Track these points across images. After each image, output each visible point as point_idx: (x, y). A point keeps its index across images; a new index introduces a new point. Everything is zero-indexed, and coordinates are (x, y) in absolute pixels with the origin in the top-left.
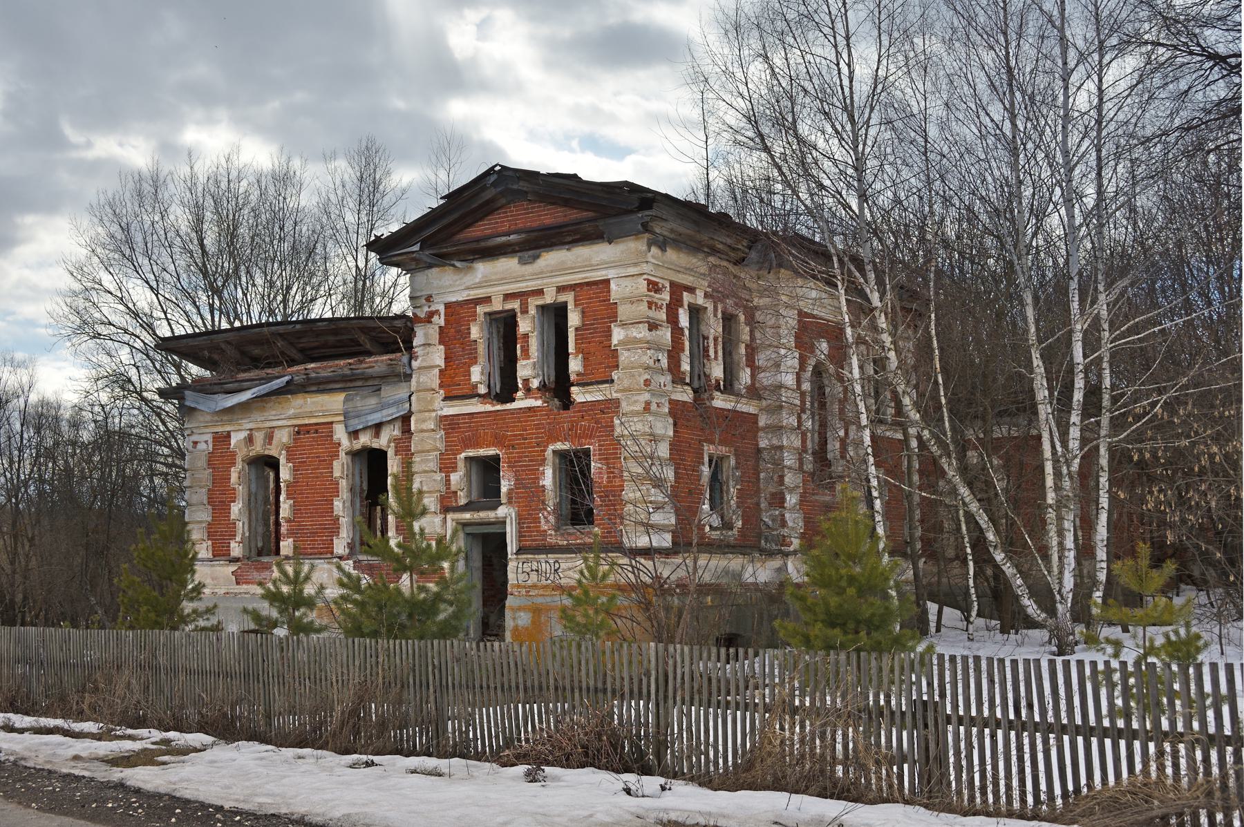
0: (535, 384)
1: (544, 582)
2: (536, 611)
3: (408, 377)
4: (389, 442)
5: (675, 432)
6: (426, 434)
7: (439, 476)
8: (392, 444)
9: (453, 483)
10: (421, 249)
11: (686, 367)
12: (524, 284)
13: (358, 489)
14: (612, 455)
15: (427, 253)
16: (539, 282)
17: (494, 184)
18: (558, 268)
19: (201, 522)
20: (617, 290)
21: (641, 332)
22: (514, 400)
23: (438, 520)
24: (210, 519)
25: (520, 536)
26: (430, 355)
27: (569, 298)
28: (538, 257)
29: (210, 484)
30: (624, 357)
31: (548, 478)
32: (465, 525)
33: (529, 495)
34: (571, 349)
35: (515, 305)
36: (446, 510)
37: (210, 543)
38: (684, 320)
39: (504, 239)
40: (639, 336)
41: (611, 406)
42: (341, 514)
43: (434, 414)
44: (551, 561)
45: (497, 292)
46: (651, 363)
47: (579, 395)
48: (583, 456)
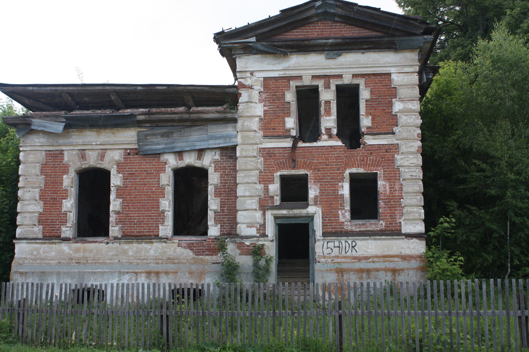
3: (235, 121)
4: (211, 163)
6: (250, 159)
7: (260, 187)
8: (213, 165)
12: (329, 71)
16: (340, 70)
18: (350, 65)
24: (41, 210)
25: (324, 225)
29: (42, 186)
31: (345, 190)
33: (330, 202)
40: (413, 108)
42: (167, 209)
43: (255, 147)
44: (350, 242)
48: (372, 179)
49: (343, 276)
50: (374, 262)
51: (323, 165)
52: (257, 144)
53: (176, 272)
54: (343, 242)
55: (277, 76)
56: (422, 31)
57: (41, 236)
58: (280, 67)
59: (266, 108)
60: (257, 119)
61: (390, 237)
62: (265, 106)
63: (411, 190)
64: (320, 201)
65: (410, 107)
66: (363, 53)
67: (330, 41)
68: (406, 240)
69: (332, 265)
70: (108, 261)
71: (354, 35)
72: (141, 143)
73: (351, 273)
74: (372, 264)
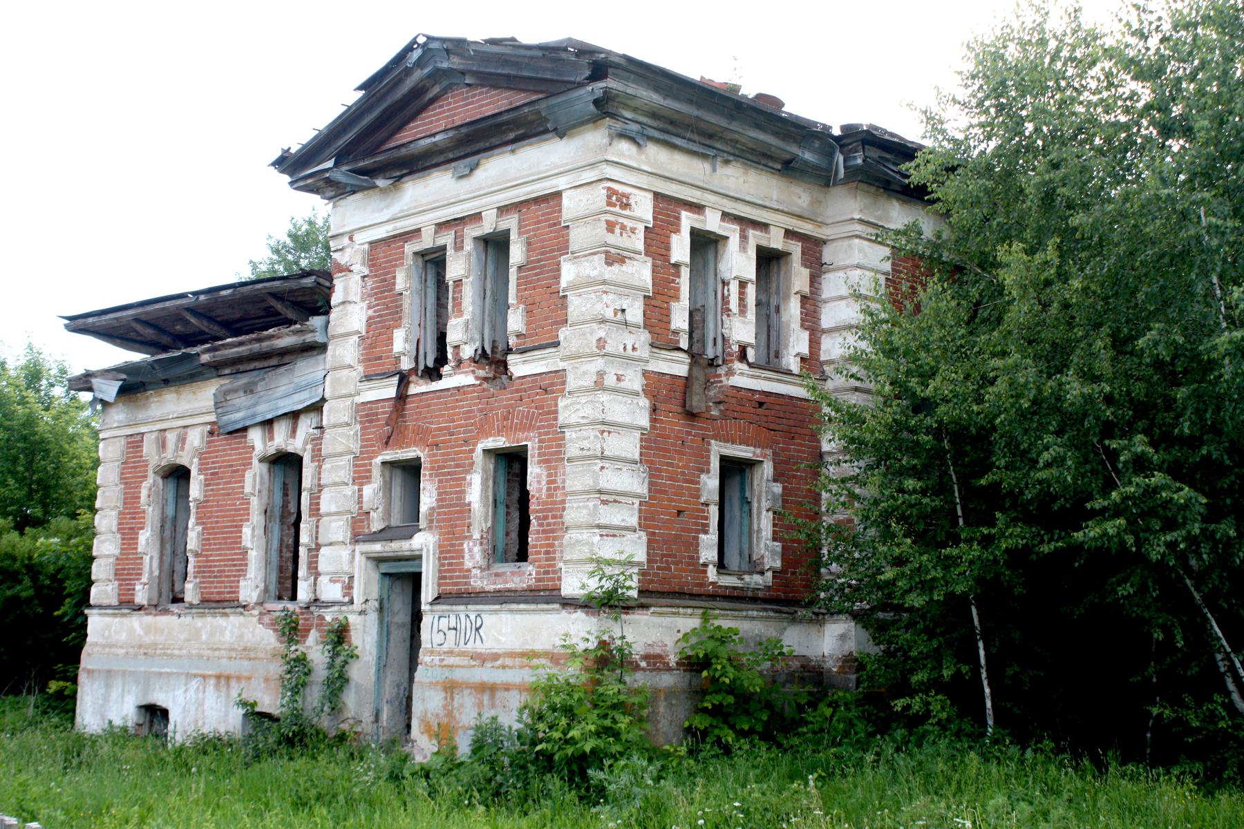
0: (468, 352)
1: (462, 647)
2: (451, 688)
4: (305, 443)
5: (653, 420)
6: (340, 430)
7: (349, 490)
9: (365, 499)
10: (336, 165)
11: (680, 320)
13: (277, 512)
14: (554, 458)
15: (344, 168)
17: (420, 63)
19: (108, 556)
20: (571, 205)
21: (595, 268)
22: (440, 377)
23: (345, 553)
26: (350, 311)
27: (510, 222)
28: (477, 165)
29: (120, 504)
30: (577, 306)
32: (379, 560)
34: (512, 300)
35: (447, 239)
36: (356, 538)
37: (117, 583)
38: (680, 249)
39: (428, 141)
41: (552, 384)
42: (249, 545)
43: (348, 402)
45: (427, 222)
46: (609, 314)
47: (519, 367)
49: (452, 699)
50: (504, 667)
51: (445, 435)
52: (351, 395)
53: (249, 678)
54: (463, 617)
55: (384, 235)
56: (587, 73)
57: (115, 602)
58: (386, 215)
59: (370, 312)
60: (355, 338)
61: (533, 607)
62: (369, 307)
63: (579, 488)
64: (438, 521)
65: (587, 272)
66: (513, 151)
67: (438, 138)
68: (564, 613)
69: (439, 670)
70: (177, 652)
71: (489, 111)
72: (219, 411)
73: (466, 692)
74: (500, 671)
